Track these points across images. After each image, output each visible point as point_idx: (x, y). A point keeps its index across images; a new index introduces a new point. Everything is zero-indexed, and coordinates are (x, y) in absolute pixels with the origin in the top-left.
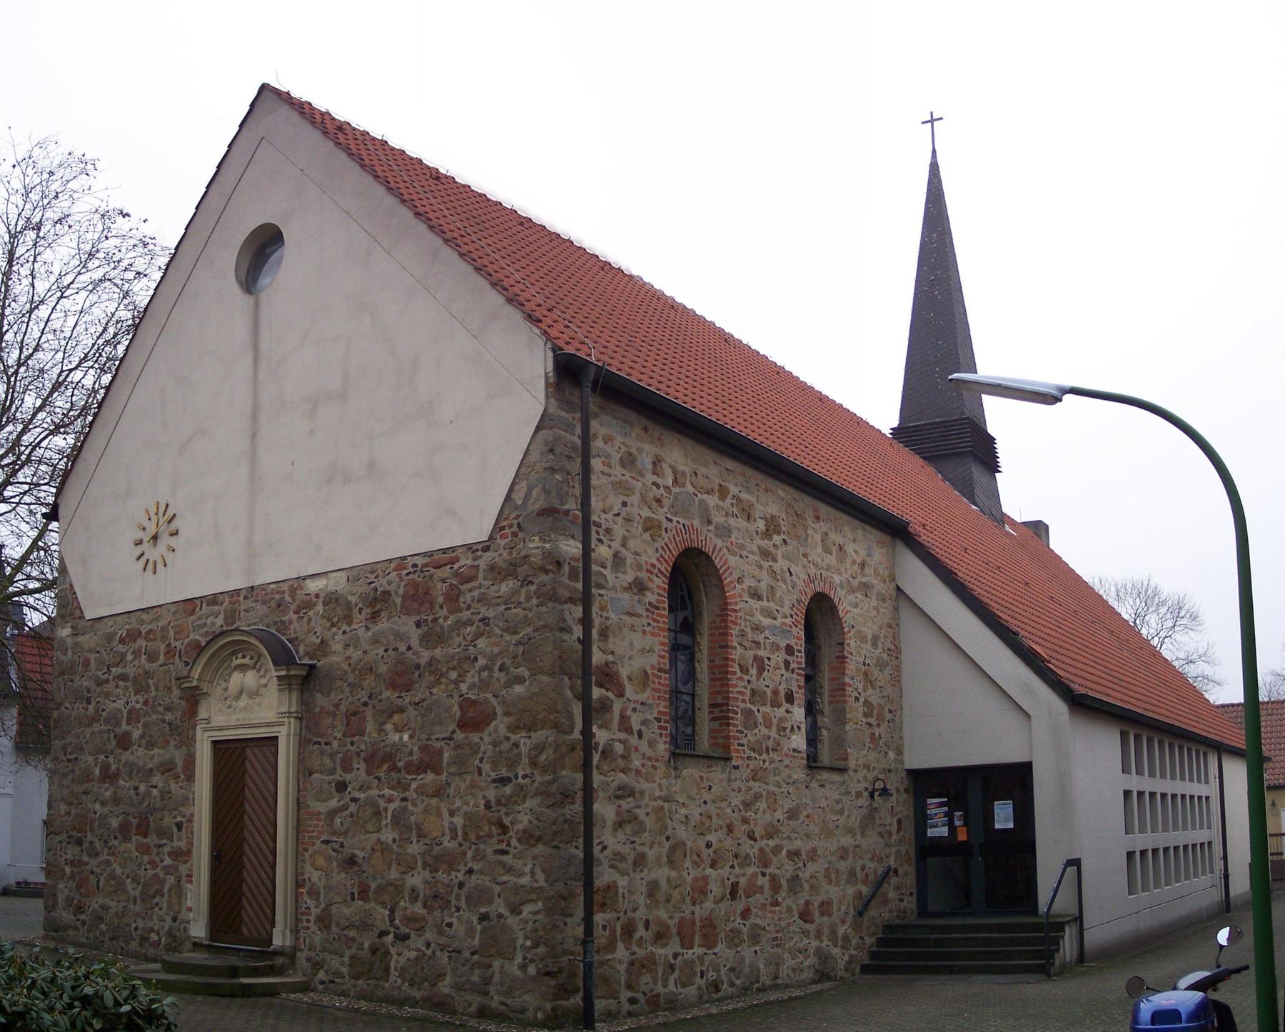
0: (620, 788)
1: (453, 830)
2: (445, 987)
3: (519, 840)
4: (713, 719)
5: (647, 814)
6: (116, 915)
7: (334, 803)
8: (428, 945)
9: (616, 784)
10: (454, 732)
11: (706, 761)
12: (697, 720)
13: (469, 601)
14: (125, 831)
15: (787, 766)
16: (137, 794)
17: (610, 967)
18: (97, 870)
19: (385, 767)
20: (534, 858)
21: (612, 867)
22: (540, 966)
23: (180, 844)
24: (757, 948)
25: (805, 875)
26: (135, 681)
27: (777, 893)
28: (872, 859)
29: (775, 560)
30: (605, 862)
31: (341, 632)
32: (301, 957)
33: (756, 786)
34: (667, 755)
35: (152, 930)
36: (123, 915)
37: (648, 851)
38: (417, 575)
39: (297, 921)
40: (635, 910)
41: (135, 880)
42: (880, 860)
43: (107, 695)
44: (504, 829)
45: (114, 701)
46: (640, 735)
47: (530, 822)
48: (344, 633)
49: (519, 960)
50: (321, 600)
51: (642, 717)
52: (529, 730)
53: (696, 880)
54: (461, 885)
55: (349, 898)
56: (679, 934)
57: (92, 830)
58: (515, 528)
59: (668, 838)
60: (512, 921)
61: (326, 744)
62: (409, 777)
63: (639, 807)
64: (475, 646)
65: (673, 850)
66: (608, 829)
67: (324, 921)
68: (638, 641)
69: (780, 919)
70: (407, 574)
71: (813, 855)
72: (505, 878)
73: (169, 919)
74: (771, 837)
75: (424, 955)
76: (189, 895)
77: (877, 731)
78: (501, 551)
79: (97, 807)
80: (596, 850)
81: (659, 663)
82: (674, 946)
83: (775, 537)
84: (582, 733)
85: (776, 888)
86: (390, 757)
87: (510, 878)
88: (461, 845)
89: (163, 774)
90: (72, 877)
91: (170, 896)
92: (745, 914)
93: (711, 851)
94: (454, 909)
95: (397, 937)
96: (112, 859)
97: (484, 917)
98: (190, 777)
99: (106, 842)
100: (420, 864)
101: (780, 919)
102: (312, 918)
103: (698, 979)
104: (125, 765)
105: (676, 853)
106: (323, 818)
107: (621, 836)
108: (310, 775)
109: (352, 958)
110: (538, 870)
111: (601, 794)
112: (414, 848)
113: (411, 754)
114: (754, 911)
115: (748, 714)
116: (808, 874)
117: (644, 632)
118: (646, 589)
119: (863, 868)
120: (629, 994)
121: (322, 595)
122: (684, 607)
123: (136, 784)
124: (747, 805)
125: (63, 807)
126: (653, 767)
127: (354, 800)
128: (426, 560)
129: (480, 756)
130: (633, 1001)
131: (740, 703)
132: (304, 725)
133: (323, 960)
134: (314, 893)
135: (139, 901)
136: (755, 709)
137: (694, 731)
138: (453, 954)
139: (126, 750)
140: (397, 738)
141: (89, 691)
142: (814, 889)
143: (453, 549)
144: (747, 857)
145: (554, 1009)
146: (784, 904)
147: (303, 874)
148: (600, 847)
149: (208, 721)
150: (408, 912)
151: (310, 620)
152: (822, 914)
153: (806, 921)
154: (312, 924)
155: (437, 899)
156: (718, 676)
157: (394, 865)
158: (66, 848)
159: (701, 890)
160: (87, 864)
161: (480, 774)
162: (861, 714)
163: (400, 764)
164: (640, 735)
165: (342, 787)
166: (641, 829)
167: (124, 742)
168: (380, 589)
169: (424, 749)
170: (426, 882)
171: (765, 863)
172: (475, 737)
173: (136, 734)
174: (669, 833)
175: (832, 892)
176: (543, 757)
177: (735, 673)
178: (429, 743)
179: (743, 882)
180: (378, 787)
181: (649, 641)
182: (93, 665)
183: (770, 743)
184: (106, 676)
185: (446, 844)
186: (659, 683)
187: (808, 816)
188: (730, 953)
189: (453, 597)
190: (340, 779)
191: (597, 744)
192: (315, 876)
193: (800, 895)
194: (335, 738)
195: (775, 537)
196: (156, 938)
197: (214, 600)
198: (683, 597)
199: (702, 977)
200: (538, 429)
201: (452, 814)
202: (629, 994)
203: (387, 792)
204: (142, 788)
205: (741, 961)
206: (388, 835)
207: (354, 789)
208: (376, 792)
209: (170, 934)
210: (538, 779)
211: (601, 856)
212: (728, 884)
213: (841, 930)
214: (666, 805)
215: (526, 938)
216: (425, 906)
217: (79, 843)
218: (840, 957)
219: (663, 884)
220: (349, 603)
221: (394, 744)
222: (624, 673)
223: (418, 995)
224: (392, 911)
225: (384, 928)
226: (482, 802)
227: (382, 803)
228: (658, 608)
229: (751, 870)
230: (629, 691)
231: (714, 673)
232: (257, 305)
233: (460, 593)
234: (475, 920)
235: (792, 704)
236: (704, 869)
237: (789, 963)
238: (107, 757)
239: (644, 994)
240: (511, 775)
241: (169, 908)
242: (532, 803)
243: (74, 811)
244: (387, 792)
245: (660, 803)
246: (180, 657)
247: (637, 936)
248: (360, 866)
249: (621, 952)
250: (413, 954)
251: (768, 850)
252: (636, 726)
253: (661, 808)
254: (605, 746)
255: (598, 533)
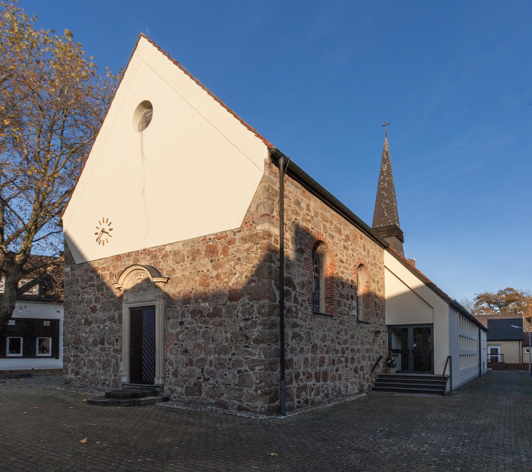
0: (293, 324)
1: (227, 339)
2: (224, 398)
3: (254, 342)
4: (327, 303)
5: (304, 334)
6: (92, 375)
7: (179, 330)
8: (217, 382)
9: (292, 322)
10: (226, 302)
11: (325, 316)
12: (321, 303)
13: (232, 252)
14: (95, 343)
15: (351, 320)
16: (100, 329)
17: (290, 390)
18: (84, 358)
19: (199, 315)
20: (260, 348)
21: (291, 352)
22: (263, 390)
23: (117, 347)
24: (341, 382)
25: (355, 357)
26: (98, 287)
27: (347, 363)
28: (376, 353)
29: (348, 250)
30: (289, 351)
31: (180, 265)
32: (166, 388)
33: (341, 326)
34: (311, 313)
35: (106, 380)
36: (95, 375)
37: (305, 348)
38: (211, 242)
39: (165, 374)
40: (299, 368)
41: (100, 361)
42: (378, 353)
43: (86, 292)
44: (247, 338)
45: (89, 295)
46: (301, 305)
47: (258, 335)
48: (182, 265)
49: (254, 388)
50: (172, 253)
51: (302, 298)
52: (258, 301)
53: (321, 358)
54: (230, 359)
55: (185, 365)
56: (315, 377)
57: (81, 343)
58: (251, 223)
59: (311, 343)
60: (251, 373)
61: (175, 307)
62: (208, 319)
63: (301, 331)
64: (235, 269)
65: (313, 347)
66: (290, 339)
67: (175, 374)
68: (302, 271)
69: (348, 372)
70: (207, 242)
71: (358, 351)
72: (248, 356)
73: (113, 376)
74: (346, 344)
75: (216, 386)
76: (121, 366)
77: (378, 312)
78: (246, 232)
79: (84, 335)
80: (285, 346)
81: (309, 280)
82: (313, 381)
83: (348, 242)
84: (279, 302)
85: (347, 361)
86: (201, 312)
87: (250, 356)
88: (230, 344)
89: (110, 321)
90: (74, 361)
91: (114, 367)
92: (337, 370)
93: (326, 348)
94: (227, 369)
95: (204, 379)
96: (90, 354)
97: (239, 372)
98: (121, 321)
99: (87, 347)
100: (213, 351)
101: (348, 372)
102: (171, 373)
103: (321, 393)
104: (94, 318)
105: (315, 348)
106: (174, 335)
107: (294, 341)
108: (169, 319)
109: (186, 387)
110: (261, 353)
111: (287, 326)
112: (212, 346)
113: (209, 310)
114: (340, 369)
115: (339, 302)
116: (356, 357)
117: (303, 268)
118: (304, 252)
119: (373, 356)
120: (298, 400)
121: (172, 252)
122: (316, 263)
123: (99, 325)
124: (338, 333)
125: (69, 336)
126: (306, 317)
127: (186, 328)
128: (215, 236)
129: (237, 310)
130: (299, 402)
131: (336, 298)
132: (166, 301)
133: (175, 389)
134: (171, 364)
135: (101, 369)
136: (341, 300)
137: (319, 307)
138: (227, 386)
139: (95, 313)
140: (203, 305)
141: (78, 291)
142: (359, 362)
143: (226, 232)
144: (338, 350)
145: (269, 407)
146: (349, 367)
147: (166, 356)
148: (287, 345)
149: (127, 300)
150: (209, 370)
151: (167, 261)
152: (361, 370)
153: (356, 373)
154: (170, 375)
155: (221, 364)
156: (328, 288)
157: (203, 352)
158: (71, 351)
159: (322, 362)
160: (80, 356)
161: (237, 317)
162: (373, 306)
163: (205, 314)
164: (301, 305)
165: (182, 323)
166: (302, 339)
167: (94, 310)
168: (196, 249)
169: (214, 308)
170: (216, 358)
171: (343, 352)
172: (235, 303)
173: (99, 307)
174: (312, 341)
175: (363, 363)
176: (263, 311)
177: (335, 287)
178: (217, 306)
179: (336, 359)
180: (196, 323)
181: (304, 272)
182: (80, 281)
183: (346, 312)
184: (86, 285)
185: (224, 344)
186: (309, 287)
187: (357, 338)
188: (332, 384)
189: (225, 251)
190: (181, 320)
191: (286, 307)
192: (171, 357)
193: (354, 364)
194: (179, 305)
195: (348, 242)
196: (108, 383)
197: (129, 255)
198: (316, 260)
199: (322, 393)
200: (260, 183)
201: (226, 332)
202: (298, 400)
203: (200, 325)
204: (102, 327)
205: (336, 386)
206: (201, 341)
207: (186, 324)
208: (195, 325)
209: (114, 381)
210: (261, 318)
211: (287, 348)
212: (332, 359)
213: (366, 376)
214: (311, 331)
215: (257, 379)
216: (215, 367)
217: (77, 348)
218: (366, 385)
219: (310, 359)
220: (183, 254)
221: (203, 307)
222: (295, 282)
223: (213, 401)
224: (202, 369)
225: (199, 376)
226: (238, 328)
227: (198, 329)
228: (308, 260)
229: (339, 355)
230: (298, 289)
231: (327, 287)
232: (142, 134)
233: (229, 249)
234: (236, 373)
235: (353, 300)
236: (324, 354)
237: (350, 387)
238: (87, 316)
239: (303, 399)
240: (250, 317)
241: (113, 371)
242: (259, 328)
243: (74, 336)
244: (200, 325)
245: (309, 330)
246: (115, 277)
247: (300, 378)
248: (189, 353)
249: (294, 384)
250: (211, 386)
251: (345, 348)
252: (300, 302)
253: (309, 332)
254: (288, 307)
255: (285, 228)
